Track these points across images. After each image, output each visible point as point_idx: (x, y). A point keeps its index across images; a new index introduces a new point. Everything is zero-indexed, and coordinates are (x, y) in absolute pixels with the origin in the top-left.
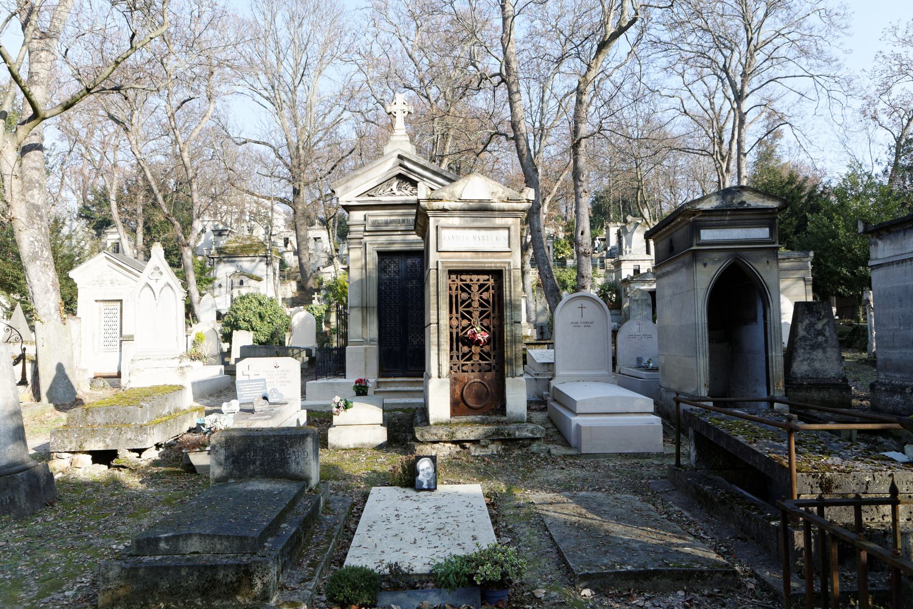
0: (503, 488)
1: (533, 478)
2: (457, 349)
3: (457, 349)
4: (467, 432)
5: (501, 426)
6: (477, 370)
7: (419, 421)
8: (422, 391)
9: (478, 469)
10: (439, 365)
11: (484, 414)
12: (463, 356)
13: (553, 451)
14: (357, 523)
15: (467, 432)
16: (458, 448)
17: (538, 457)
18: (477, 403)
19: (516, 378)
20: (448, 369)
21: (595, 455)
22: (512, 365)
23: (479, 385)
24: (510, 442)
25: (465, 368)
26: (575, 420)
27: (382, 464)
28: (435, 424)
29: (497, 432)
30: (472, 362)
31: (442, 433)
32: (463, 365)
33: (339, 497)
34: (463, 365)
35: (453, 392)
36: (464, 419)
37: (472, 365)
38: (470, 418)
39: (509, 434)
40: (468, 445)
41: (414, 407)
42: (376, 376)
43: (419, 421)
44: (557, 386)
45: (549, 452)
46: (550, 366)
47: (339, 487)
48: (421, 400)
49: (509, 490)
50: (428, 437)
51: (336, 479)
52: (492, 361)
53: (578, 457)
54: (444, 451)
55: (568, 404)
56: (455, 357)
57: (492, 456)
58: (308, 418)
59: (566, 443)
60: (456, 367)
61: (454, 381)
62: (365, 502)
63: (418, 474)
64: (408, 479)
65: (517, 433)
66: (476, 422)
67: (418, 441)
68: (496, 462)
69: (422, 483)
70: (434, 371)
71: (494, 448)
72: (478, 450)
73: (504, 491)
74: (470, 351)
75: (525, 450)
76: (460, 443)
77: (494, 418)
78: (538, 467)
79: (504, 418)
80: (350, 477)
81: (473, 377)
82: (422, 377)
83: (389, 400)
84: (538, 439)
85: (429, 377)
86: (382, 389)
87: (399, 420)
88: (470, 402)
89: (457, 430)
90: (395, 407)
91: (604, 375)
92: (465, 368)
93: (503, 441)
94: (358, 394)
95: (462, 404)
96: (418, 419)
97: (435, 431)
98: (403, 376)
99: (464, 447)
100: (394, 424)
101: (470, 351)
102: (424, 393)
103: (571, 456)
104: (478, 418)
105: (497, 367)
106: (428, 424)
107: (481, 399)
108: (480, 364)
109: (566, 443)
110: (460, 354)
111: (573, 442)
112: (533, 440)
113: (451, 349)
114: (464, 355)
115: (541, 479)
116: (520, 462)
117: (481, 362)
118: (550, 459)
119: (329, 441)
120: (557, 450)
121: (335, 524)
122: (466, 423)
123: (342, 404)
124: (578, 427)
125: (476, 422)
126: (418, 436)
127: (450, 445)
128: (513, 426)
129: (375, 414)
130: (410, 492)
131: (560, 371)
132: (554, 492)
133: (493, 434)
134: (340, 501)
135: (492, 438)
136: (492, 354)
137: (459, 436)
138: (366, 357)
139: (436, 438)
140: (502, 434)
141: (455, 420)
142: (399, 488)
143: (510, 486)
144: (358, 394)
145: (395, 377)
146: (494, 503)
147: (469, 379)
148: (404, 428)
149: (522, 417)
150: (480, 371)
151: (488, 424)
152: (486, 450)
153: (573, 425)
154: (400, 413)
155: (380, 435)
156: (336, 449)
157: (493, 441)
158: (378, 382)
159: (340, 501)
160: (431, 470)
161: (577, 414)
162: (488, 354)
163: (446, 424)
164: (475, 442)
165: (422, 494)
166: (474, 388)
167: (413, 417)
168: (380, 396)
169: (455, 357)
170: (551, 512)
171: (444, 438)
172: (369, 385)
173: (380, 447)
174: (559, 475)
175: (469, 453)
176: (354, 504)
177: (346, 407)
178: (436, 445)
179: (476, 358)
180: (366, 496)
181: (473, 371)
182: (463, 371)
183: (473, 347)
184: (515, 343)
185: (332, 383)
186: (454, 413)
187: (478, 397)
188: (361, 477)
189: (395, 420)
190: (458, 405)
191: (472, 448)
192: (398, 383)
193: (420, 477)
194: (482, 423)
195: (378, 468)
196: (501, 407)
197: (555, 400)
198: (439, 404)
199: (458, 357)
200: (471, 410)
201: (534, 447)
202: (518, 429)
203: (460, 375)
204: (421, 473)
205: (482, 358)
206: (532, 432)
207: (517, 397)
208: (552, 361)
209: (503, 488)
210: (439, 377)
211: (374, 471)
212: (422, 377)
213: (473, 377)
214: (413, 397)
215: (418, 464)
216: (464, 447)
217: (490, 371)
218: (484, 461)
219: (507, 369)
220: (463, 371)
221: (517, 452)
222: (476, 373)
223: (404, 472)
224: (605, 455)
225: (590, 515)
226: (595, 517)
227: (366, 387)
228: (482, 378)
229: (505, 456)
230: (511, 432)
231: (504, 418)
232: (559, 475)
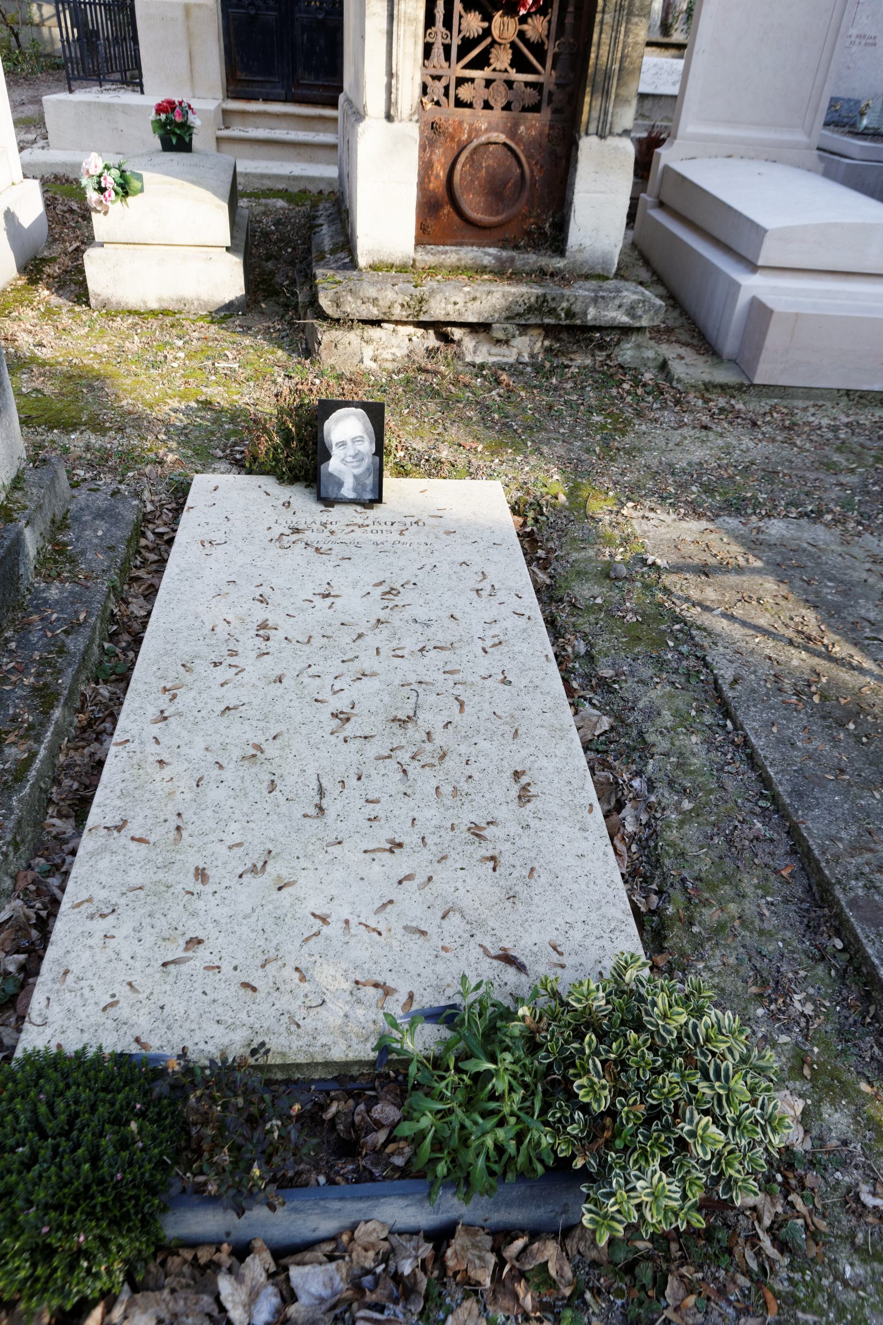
0: (554, 484)
1: (631, 452)
2: (448, 23)
3: (448, 23)
4: (460, 300)
5: (551, 289)
6: (498, 103)
7: (327, 244)
8: (334, 147)
9: (485, 409)
10: (390, 75)
11: (504, 244)
12: (464, 49)
13: (678, 369)
14: (151, 593)
15: (460, 300)
16: (432, 341)
17: (637, 382)
18: (490, 210)
19: (612, 141)
20: (418, 90)
21: (783, 391)
22: (606, 94)
23: (501, 150)
24: (569, 333)
25: (465, 93)
26: (753, 285)
27: (229, 376)
28: (374, 267)
29: (540, 306)
30: (486, 73)
31: (392, 296)
32: (460, 81)
33: (101, 501)
34: (460, 81)
35: (426, 168)
36: (452, 255)
37: (489, 83)
38: (469, 254)
39: (570, 314)
40: (457, 333)
41: (313, 188)
42: (220, 95)
43: (327, 244)
44: (681, 167)
45: (663, 366)
46: (670, 103)
47: (105, 456)
48: (331, 172)
49: (572, 494)
50: (353, 307)
51: (98, 427)
52: (546, 75)
53: (740, 394)
54: (394, 347)
55: (737, 239)
56: (438, 51)
57: (515, 369)
58: (50, 204)
59: (705, 344)
60: (439, 86)
61: (433, 132)
62: (178, 511)
63: (328, 456)
64: (297, 456)
65: (592, 312)
66: (482, 270)
67: (322, 316)
68: (528, 387)
69: (340, 484)
70: (373, 98)
71: (525, 347)
72: (484, 349)
73: (562, 498)
74: (487, 32)
75: (601, 356)
76: (440, 328)
77: (532, 259)
78: (639, 414)
79: (559, 263)
80: (133, 422)
81: (486, 126)
82: (334, 105)
83: (253, 165)
84: (640, 329)
85: (359, 115)
86: (235, 132)
87: (277, 223)
88: (473, 205)
89: (432, 292)
90: (269, 184)
91: (793, 146)
92: (465, 93)
93: (549, 331)
94: (167, 147)
95: (447, 209)
96: (326, 236)
97: (372, 292)
98: (286, 100)
99: (446, 339)
100: (266, 234)
101: (487, 32)
102: (340, 152)
103: (723, 388)
104: (488, 255)
105: (558, 96)
106: (353, 265)
107: (508, 205)
108: (510, 84)
109: (705, 344)
110: (456, 42)
111: (729, 346)
112: (626, 331)
113: (430, 21)
114: (467, 45)
115: (652, 459)
116: (591, 395)
117: (514, 75)
118: (665, 387)
119: (93, 285)
120: (689, 368)
121: (73, 628)
122: (456, 270)
123: (109, 181)
124: (760, 313)
125: (482, 270)
126: (324, 302)
127: (410, 329)
128: (581, 291)
129: (212, 218)
130: (300, 498)
131: (690, 124)
132: (700, 516)
133: (530, 309)
134: (100, 515)
135: (521, 319)
136: (551, 49)
137: (438, 310)
138: (189, 35)
139: (375, 313)
140: (552, 312)
141: (426, 257)
142: (268, 482)
143: (577, 473)
144: (167, 147)
145: (266, 100)
146: (541, 536)
147: (474, 132)
148: (289, 254)
149: (606, 262)
150: (507, 107)
151: (516, 276)
152: (504, 349)
153: (743, 299)
154: (280, 203)
155: (227, 280)
156: (112, 311)
157: (524, 329)
158: (225, 112)
159: (100, 515)
160: (368, 447)
161: (753, 267)
162: (538, 49)
163: (403, 269)
164: (479, 328)
165: (338, 513)
166: (487, 162)
167: (310, 226)
168: (227, 157)
169: (438, 51)
170: (700, 599)
171: (398, 313)
172: (195, 120)
173: (225, 314)
174: (696, 451)
175: (458, 356)
176: (146, 519)
177: (125, 189)
178: (374, 332)
179: (502, 59)
180: (180, 492)
181: (487, 106)
182: (459, 103)
183: (497, 18)
184: (630, 14)
185: (108, 106)
186: (425, 235)
187: (496, 191)
188: (167, 424)
189: (268, 223)
190: (441, 213)
191: (469, 342)
192: (275, 119)
193: (334, 465)
194: (501, 272)
195: (218, 395)
196: (553, 232)
197: (661, 205)
198: (385, 214)
199: (447, 48)
200: (473, 230)
201: (627, 353)
202: (595, 300)
203: (450, 114)
204: (336, 452)
205: (519, 63)
206: (631, 311)
207: (600, 206)
208: (674, 90)
209: (554, 484)
210: (389, 118)
211: (207, 405)
212: (334, 105)
213: (486, 126)
214: (311, 160)
215: (327, 424)
216: (446, 339)
217: (535, 108)
218: (499, 383)
219: (590, 107)
220: (459, 103)
221: (581, 360)
222: (497, 114)
223: (287, 438)
224: (809, 393)
225: (841, 650)
226: (858, 658)
227: (186, 127)
228: (512, 133)
229: (552, 371)
230: (577, 308)
231: (559, 263)
232: (696, 451)
